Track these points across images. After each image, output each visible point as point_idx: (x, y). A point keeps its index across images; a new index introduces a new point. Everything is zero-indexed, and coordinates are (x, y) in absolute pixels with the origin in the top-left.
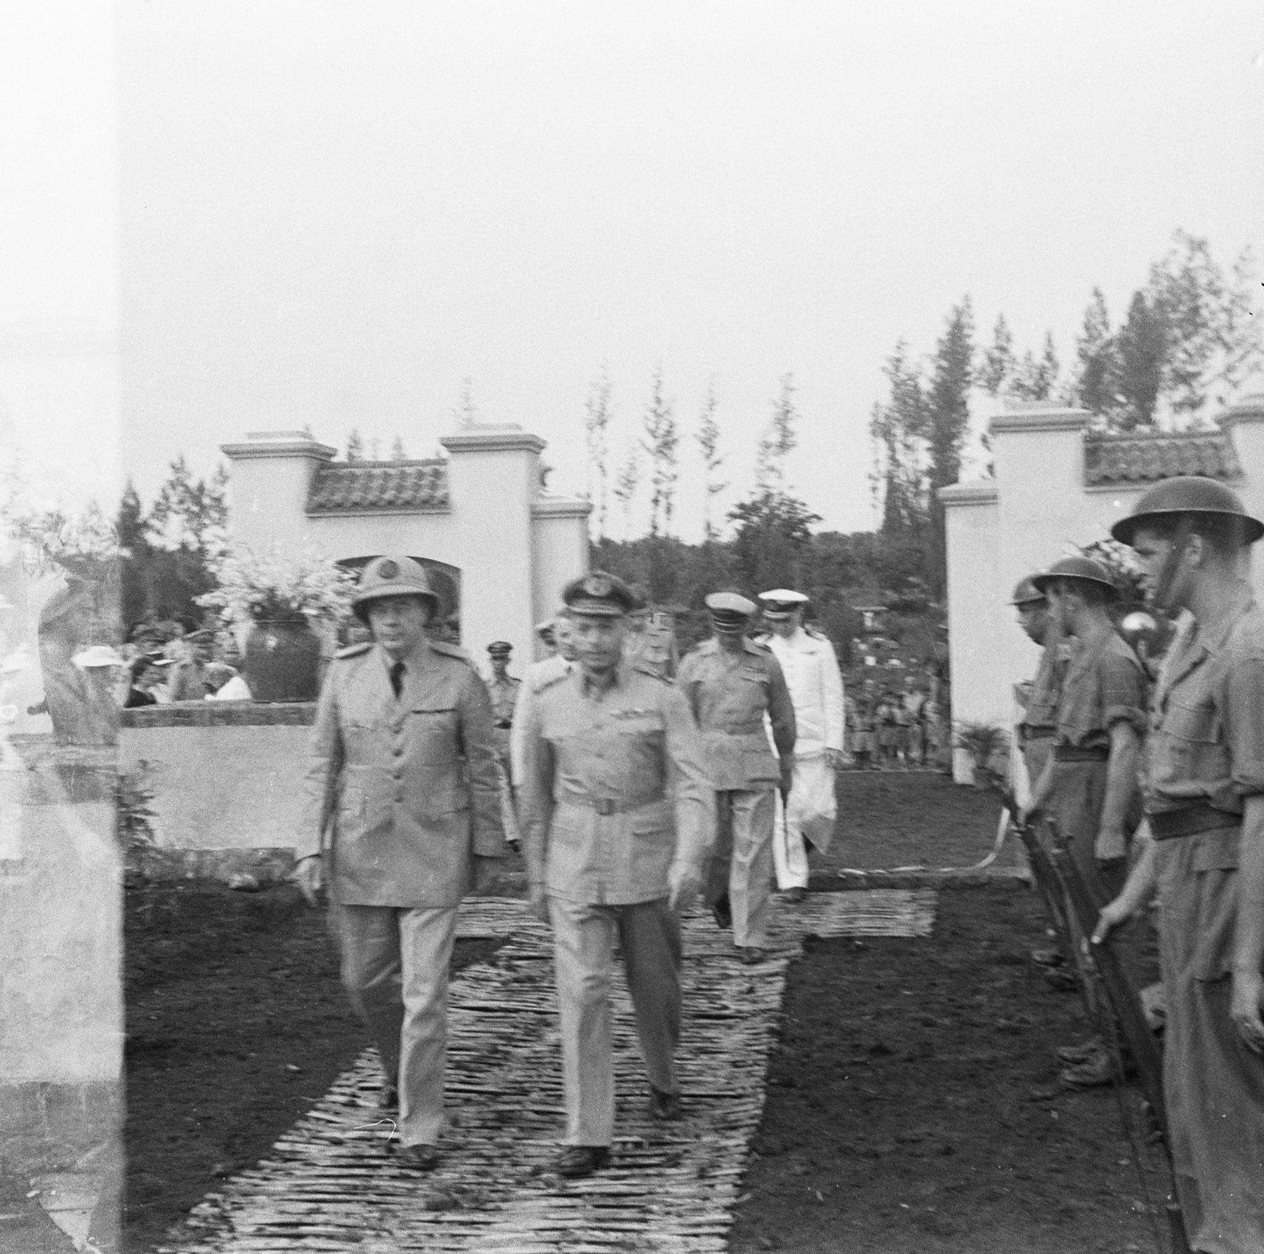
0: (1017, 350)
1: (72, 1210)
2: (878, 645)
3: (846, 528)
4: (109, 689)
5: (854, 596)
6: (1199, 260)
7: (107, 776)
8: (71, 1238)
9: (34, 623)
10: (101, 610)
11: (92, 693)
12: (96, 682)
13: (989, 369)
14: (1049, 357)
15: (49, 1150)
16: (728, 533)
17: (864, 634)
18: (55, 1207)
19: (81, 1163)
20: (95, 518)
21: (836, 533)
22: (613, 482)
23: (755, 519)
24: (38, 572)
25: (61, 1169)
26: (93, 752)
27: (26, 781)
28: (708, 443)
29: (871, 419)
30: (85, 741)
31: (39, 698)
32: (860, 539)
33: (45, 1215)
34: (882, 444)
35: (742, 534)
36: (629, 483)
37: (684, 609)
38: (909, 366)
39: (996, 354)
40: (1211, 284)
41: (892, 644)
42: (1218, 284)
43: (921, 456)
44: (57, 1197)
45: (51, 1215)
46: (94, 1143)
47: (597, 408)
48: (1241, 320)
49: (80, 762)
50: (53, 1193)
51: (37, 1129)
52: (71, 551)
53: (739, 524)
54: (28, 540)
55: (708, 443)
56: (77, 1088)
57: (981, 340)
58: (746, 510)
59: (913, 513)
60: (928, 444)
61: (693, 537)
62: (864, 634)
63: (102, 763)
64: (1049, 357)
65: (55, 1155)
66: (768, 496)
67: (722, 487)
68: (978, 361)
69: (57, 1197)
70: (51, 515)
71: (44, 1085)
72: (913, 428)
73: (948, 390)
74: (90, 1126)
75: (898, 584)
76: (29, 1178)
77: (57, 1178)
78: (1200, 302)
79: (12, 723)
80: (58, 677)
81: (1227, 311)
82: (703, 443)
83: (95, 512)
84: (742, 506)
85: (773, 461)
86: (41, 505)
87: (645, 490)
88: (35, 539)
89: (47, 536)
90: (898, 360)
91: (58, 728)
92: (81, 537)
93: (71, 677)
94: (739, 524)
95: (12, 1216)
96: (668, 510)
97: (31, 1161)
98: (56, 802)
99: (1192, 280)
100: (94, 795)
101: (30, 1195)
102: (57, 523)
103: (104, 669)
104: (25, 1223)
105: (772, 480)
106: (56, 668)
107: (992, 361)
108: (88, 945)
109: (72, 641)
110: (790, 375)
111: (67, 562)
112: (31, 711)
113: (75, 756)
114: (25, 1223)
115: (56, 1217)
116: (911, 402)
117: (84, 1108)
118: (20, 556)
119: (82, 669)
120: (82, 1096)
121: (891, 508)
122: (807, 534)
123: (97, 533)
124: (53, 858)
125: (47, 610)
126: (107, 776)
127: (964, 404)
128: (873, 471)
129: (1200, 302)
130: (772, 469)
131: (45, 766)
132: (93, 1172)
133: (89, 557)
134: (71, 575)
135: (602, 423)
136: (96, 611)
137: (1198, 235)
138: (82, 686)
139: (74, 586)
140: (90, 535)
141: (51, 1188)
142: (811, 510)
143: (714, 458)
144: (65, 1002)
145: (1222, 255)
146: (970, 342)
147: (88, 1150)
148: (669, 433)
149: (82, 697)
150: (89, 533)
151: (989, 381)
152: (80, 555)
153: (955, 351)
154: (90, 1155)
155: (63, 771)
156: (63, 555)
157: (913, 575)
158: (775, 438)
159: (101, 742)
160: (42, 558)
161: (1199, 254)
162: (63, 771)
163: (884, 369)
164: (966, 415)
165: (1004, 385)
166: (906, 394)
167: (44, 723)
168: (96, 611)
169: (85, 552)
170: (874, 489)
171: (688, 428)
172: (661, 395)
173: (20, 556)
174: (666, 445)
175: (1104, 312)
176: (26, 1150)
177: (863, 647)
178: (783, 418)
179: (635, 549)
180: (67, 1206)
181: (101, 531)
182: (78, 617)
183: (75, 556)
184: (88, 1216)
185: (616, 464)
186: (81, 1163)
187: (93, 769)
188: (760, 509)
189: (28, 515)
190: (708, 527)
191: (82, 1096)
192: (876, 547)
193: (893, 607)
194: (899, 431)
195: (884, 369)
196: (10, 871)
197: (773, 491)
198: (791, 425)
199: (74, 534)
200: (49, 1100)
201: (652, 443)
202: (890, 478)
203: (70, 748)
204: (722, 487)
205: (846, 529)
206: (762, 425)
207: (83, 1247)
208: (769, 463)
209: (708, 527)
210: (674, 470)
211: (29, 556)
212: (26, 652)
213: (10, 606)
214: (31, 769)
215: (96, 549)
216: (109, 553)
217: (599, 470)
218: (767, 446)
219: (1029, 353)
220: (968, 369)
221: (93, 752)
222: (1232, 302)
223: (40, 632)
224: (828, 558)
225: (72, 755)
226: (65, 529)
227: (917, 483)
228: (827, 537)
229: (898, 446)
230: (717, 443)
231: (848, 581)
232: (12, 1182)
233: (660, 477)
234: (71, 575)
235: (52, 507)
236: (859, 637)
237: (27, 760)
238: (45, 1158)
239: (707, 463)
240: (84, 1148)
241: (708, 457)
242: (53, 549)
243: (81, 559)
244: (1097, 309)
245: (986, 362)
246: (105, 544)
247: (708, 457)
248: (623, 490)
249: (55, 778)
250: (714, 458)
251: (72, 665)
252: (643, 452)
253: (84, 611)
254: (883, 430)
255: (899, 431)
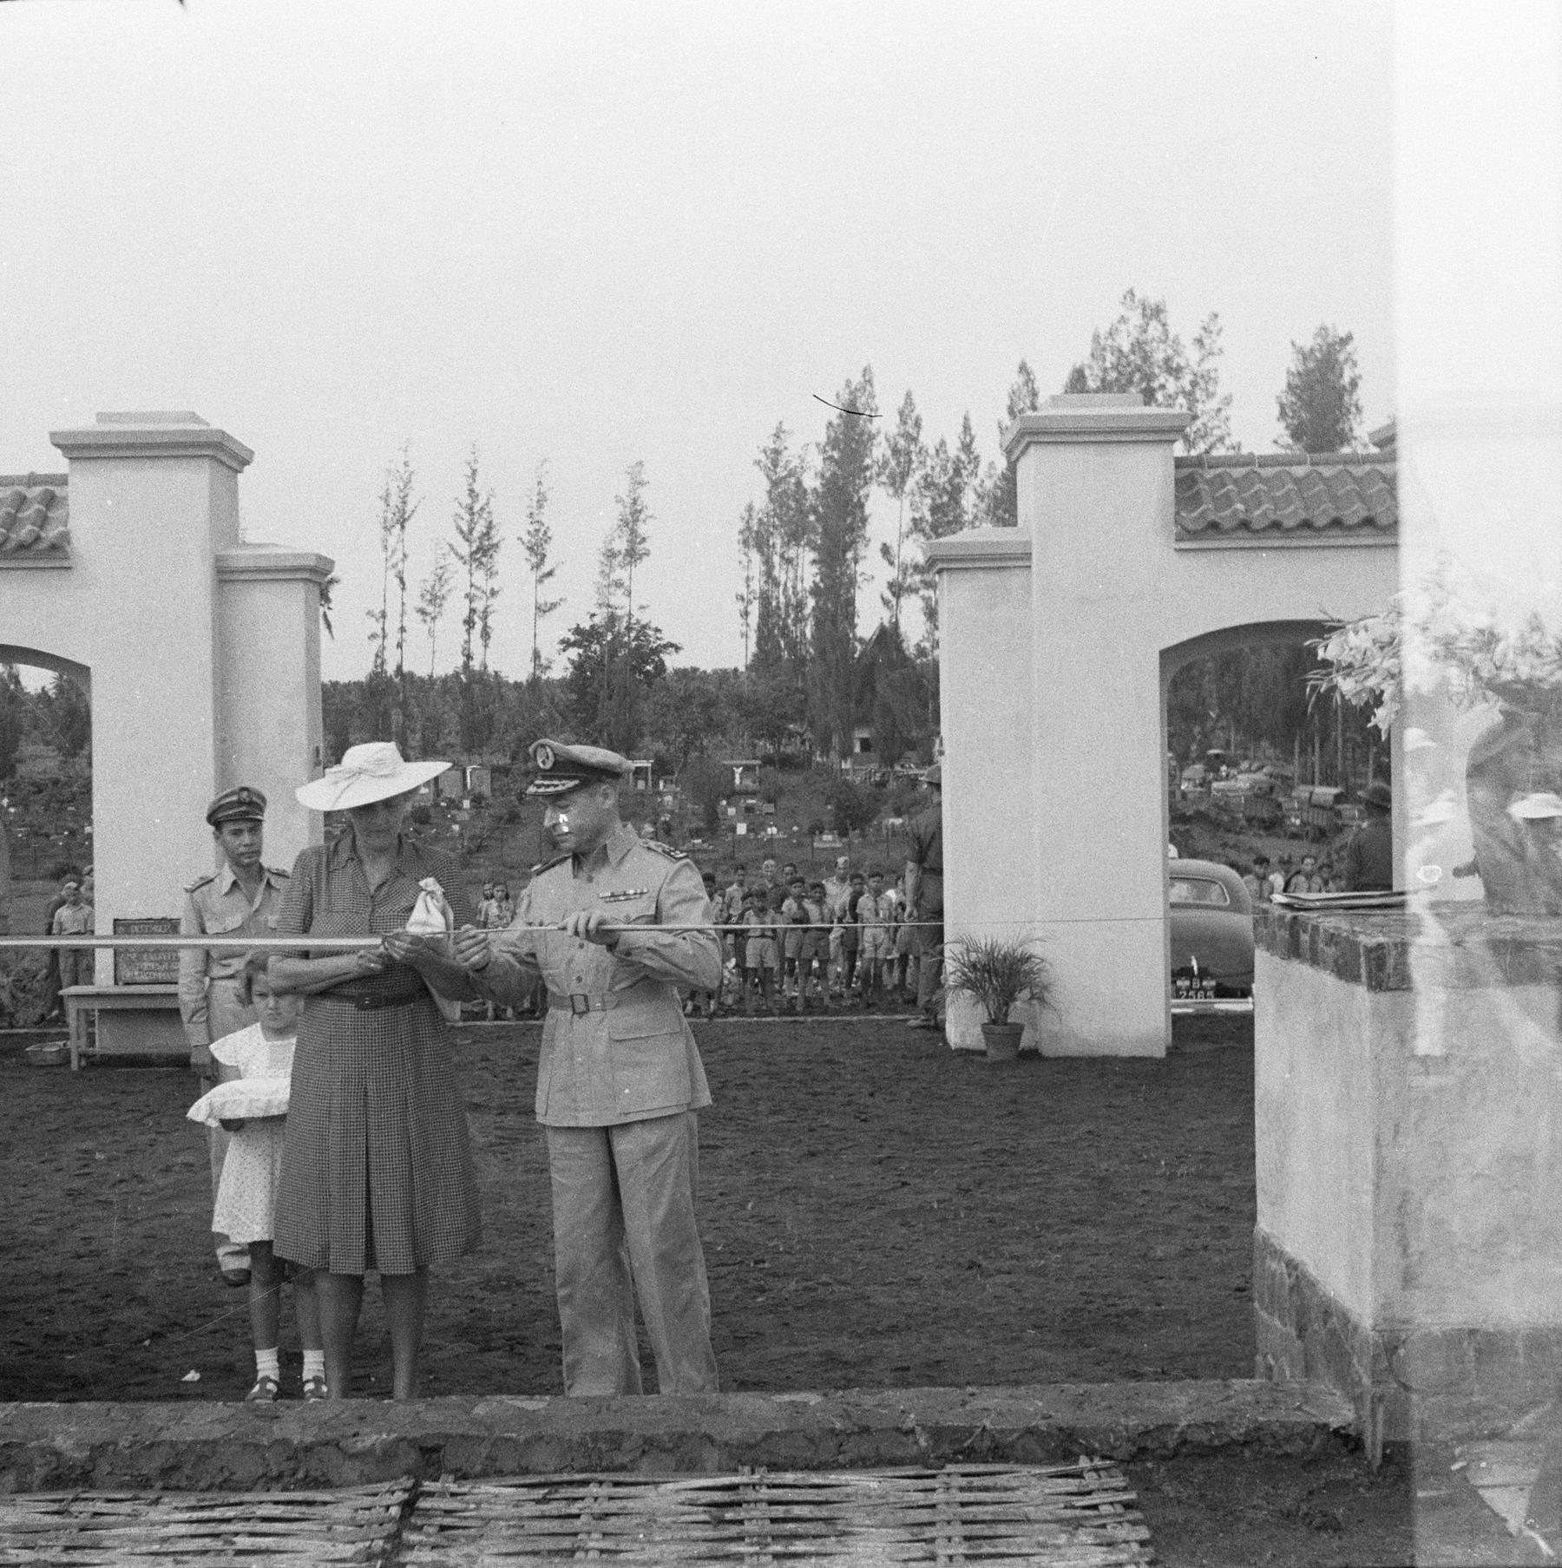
0: (928, 439)
1: (1506, 1486)
2: (749, 809)
3: (708, 663)
4: (1553, 847)
5: (718, 747)
6: (1154, 330)
7: (1550, 952)
8: (1505, 1520)
9: (1461, 765)
10: (1545, 749)
11: (1532, 850)
12: (1537, 838)
13: (893, 463)
14: (967, 448)
15: (1479, 1413)
16: (560, 668)
17: (733, 795)
18: (1485, 1482)
19: (1517, 1428)
20: (1536, 637)
21: (695, 670)
22: (414, 600)
23: (595, 647)
24: (1466, 702)
25: (1493, 1436)
26: (1534, 923)
27: (1451, 959)
28: (537, 550)
29: (742, 525)
30: (1524, 910)
31: (1467, 857)
32: (723, 676)
33: (1473, 1492)
34: (756, 557)
35: (579, 666)
36: (435, 599)
37: (502, 760)
38: (791, 457)
39: (902, 443)
40: (1167, 360)
41: (770, 808)
42: (1177, 361)
43: (806, 570)
44: (1489, 1470)
45: (1481, 1492)
46: (1534, 1404)
47: (395, 500)
48: (1205, 407)
49: (1517, 936)
50: (1483, 1464)
51: (1465, 1386)
52: (1507, 676)
53: (574, 653)
54: (1454, 662)
55: (537, 550)
56: (1514, 1335)
57: (885, 425)
58: (584, 637)
59: (793, 646)
60: (812, 555)
61: (516, 670)
62: (733, 795)
63: (1545, 937)
64: (967, 448)
65: (1486, 1418)
66: (612, 619)
67: (553, 606)
68: (879, 451)
69: (1489, 1470)
70: (1481, 632)
71: (1472, 1332)
72: (795, 537)
73: (842, 490)
74: (1529, 1382)
75: (775, 733)
76: (1453, 1447)
77: (1488, 1446)
78: (1155, 384)
79: (1433, 888)
80: (1490, 831)
81: (1189, 395)
82: (530, 549)
83: (1537, 628)
84: (578, 630)
85: (620, 574)
86: (1471, 618)
87: (456, 608)
88: (1462, 661)
89: (1477, 658)
90: (777, 452)
91: (1490, 893)
92: (1519, 660)
93: (1508, 836)
94: (574, 653)
95: (1432, 1493)
96: (486, 634)
97: (1457, 1425)
98: (1487, 985)
99: (1146, 358)
100: (1534, 976)
101: (1455, 1467)
102: (1489, 643)
103: (1547, 821)
104: (1448, 1502)
105: (618, 599)
106: (1488, 820)
107: (896, 452)
108: (1527, 1159)
109: (1508, 787)
110: (640, 464)
111: (1503, 690)
112: (1458, 873)
113: (1512, 929)
114: (1448, 1502)
115: (1486, 1494)
116: (793, 504)
117: (1521, 1360)
118: (1444, 683)
119: (1520, 821)
120: (1519, 1344)
121: (764, 637)
122: (661, 667)
123: (1539, 655)
124: (1483, 1054)
125: (1476, 749)
126: (1550, 952)
127: (861, 506)
128: (743, 591)
129: (1155, 384)
130: (619, 584)
131: (1475, 941)
132: (1533, 1439)
133: (1529, 683)
134: (1506, 706)
135: (402, 523)
136: (1537, 750)
137: (1153, 300)
138: (1521, 844)
139: (1511, 720)
140: (1529, 657)
141: (1481, 1459)
142: (667, 637)
143: (545, 569)
144: (1500, 1230)
145: (1183, 324)
146: (873, 427)
147: (1527, 1412)
148: (487, 534)
149: (1520, 856)
150: (1528, 655)
151: (892, 477)
152: (1517, 680)
153: (850, 436)
154: (1529, 1418)
155: (1497, 946)
156: (1498, 681)
157: (794, 721)
158: (621, 545)
159: (1544, 911)
160: (1471, 684)
161: (1154, 323)
162: (1497, 946)
163: (758, 463)
164: (864, 520)
165: (911, 483)
166: (785, 492)
167: (1472, 889)
168: (1537, 750)
169: (1524, 677)
170: (746, 614)
171: (511, 532)
172: (476, 487)
173: (1444, 683)
174: (483, 552)
175: (1035, 394)
176: (1450, 1414)
177: (731, 811)
178: (633, 517)
179: (447, 685)
180: (1500, 1480)
181: (1545, 652)
182: (1516, 757)
183: (1510, 682)
184: (1526, 1493)
185: (419, 574)
186: (1517, 1428)
187: (1533, 944)
188: (602, 635)
189: (1454, 632)
190: (536, 655)
191: (1519, 1344)
192: (746, 689)
193: (768, 761)
194: (777, 540)
195: (758, 463)
196: (1431, 1070)
197: (619, 612)
198: (642, 529)
199: (1511, 656)
200: (1479, 1351)
201: (465, 549)
202: (765, 599)
203: (1505, 919)
204: (553, 606)
205: (707, 665)
206: (604, 525)
207: (1520, 1531)
208: (614, 576)
209: (536, 655)
210: (494, 583)
211: (1455, 682)
212: (1451, 800)
213: (1428, 743)
214: (1458, 944)
215: (1538, 674)
216: (1553, 679)
217: (397, 581)
218: (611, 555)
219: (943, 443)
220: (868, 461)
221: (1534, 923)
222: (1194, 384)
223: (1469, 776)
224: (687, 699)
225: (1508, 927)
226: (1500, 647)
227: (800, 606)
228: (683, 674)
229: (776, 559)
230: (549, 549)
231: (712, 726)
232: (1433, 1452)
233: (473, 591)
234: (1506, 706)
235: (1483, 621)
236: (728, 798)
237: (1452, 933)
238: (1473, 1422)
239: (533, 576)
240: (1521, 1411)
241: (537, 566)
242: (1485, 674)
243: (1519, 686)
244: (1024, 390)
245: (889, 453)
246: (1548, 668)
247: (537, 566)
248: (430, 609)
249: (1488, 955)
250: (545, 569)
251: (1509, 816)
252: (452, 558)
253: (1522, 749)
254: (756, 539)
255: (777, 540)
